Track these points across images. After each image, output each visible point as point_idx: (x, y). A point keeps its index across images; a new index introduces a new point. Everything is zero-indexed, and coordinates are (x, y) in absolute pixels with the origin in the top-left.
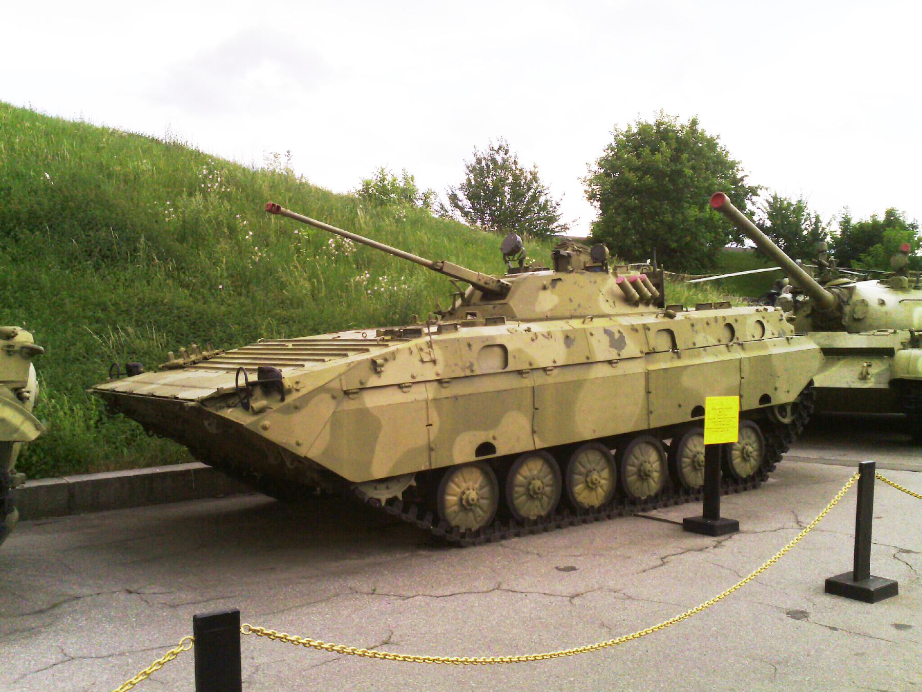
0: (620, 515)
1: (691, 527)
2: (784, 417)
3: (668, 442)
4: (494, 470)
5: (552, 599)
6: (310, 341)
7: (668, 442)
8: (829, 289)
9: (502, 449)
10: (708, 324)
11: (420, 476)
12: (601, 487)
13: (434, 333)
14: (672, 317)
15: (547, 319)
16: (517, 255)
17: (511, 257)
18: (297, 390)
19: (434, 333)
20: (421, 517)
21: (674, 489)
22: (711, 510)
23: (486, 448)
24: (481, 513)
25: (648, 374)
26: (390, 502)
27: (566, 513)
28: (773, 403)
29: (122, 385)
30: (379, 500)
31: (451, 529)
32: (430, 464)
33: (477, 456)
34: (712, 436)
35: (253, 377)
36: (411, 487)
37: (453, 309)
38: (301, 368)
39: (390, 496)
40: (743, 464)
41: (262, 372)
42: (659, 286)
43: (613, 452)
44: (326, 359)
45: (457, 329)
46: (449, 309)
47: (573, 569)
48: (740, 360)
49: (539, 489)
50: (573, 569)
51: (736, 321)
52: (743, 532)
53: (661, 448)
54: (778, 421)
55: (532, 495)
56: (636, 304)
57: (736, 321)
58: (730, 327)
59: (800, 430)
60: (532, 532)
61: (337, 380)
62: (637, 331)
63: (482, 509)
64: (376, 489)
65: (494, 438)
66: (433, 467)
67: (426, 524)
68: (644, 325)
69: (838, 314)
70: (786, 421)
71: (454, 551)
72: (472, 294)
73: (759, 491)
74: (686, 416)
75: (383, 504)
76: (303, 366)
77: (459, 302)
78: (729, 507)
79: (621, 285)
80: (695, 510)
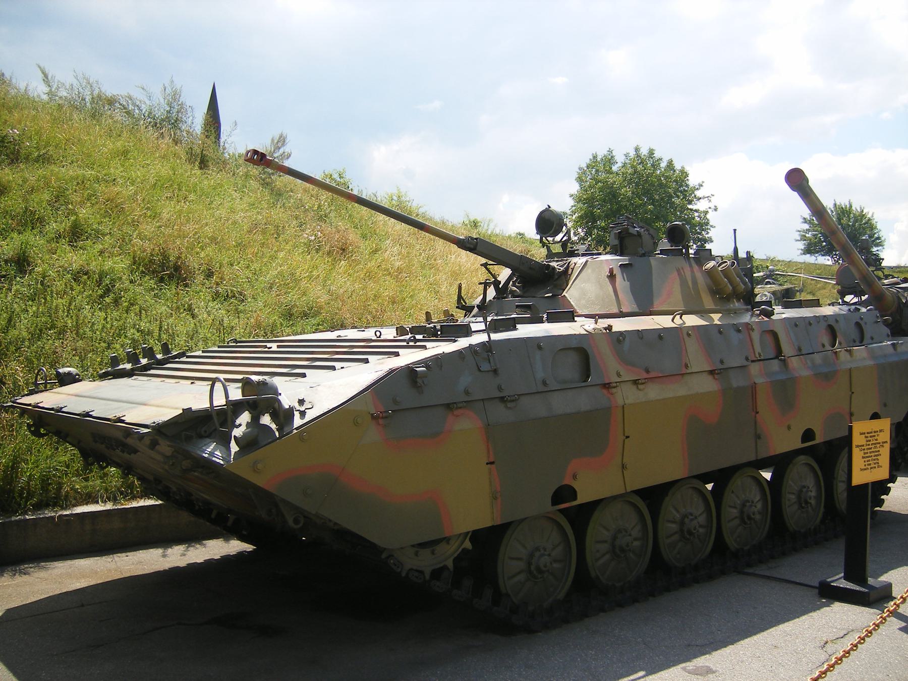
10: (356, 424)
11: (476, 536)
15: (158, 406)
23: (564, 493)
29: (49, 399)
30: (421, 572)
33: (802, 443)
35: (236, 393)
38: (300, 379)
41: (247, 384)
49: (545, 566)
55: (745, 518)
66: (759, 458)
69: (583, 401)
75: (427, 577)
76: (304, 375)
77: (491, 293)
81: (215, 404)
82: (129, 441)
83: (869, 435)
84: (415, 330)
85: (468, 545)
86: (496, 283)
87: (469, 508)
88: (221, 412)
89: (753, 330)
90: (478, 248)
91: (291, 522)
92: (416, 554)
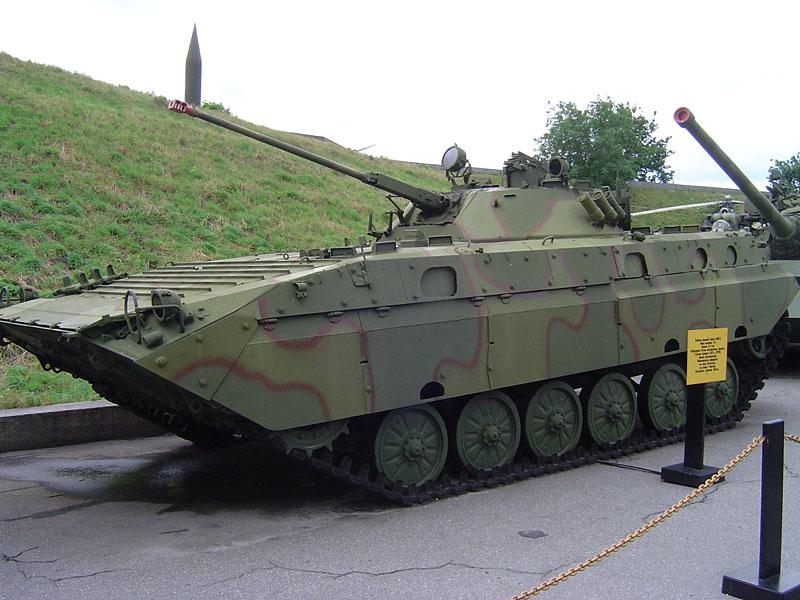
0: (587, 463)
2: (758, 351)
3: (637, 379)
4: (440, 412)
5: (520, 576)
6: (234, 263)
7: (637, 379)
9: (451, 392)
10: (680, 248)
11: (354, 422)
13: (368, 253)
14: (641, 239)
16: (462, 171)
17: (455, 174)
19: (368, 253)
20: (355, 471)
21: (646, 435)
22: (694, 456)
25: (586, 307)
26: (318, 453)
27: (527, 463)
28: (750, 335)
33: (422, 398)
36: (342, 434)
37: (390, 229)
39: (316, 447)
40: (717, 403)
43: (579, 390)
44: (238, 281)
46: (385, 229)
47: (542, 534)
48: (715, 288)
51: (709, 245)
53: (632, 388)
54: (754, 355)
56: (600, 224)
58: (703, 253)
60: (487, 486)
62: (605, 254)
64: (300, 438)
70: (761, 355)
71: (394, 512)
72: (411, 212)
73: (734, 432)
74: (658, 351)
75: (310, 454)
77: (396, 221)
79: (586, 203)
80: (675, 456)
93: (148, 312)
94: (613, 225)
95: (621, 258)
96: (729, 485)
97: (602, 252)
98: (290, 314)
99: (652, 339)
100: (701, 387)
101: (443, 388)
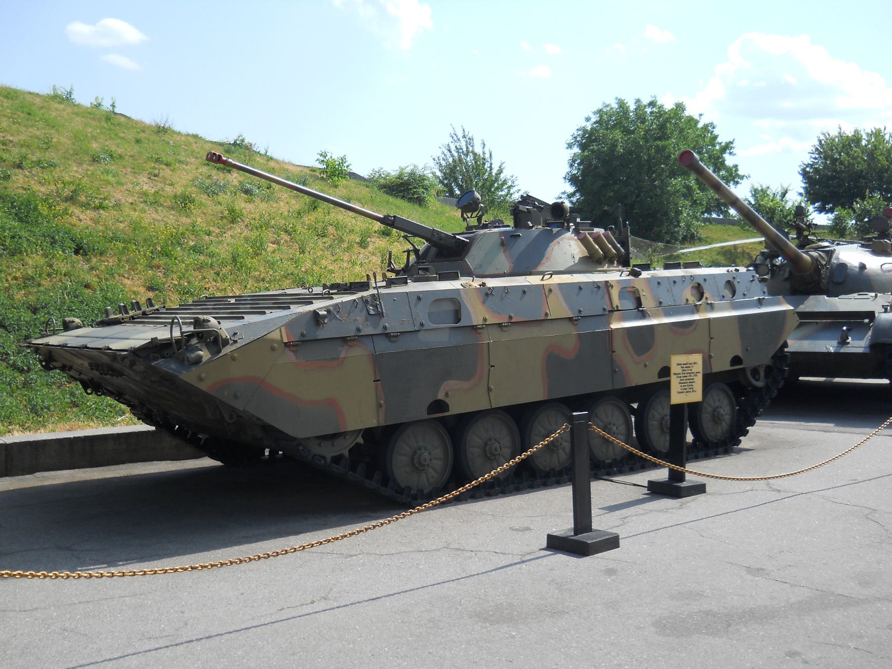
1: (657, 490)
2: (757, 380)
8: (806, 253)
9: (456, 408)
11: (368, 433)
12: (563, 449)
18: (235, 342)
23: (439, 406)
24: (434, 474)
30: (324, 458)
31: (400, 491)
32: (378, 421)
34: (677, 398)
36: (358, 444)
42: (624, 244)
45: (407, 283)
47: (528, 529)
50: (528, 529)
52: (711, 494)
54: (751, 385)
57: (705, 280)
59: (775, 393)
61: (278, 331)
63: (434, 469)
65: (447, 395)
66: (616, 388)
67: (372, 484)
68: (607, 282)
70: (760, 384)
75: (329, 460)
77: (413, 257)
78: (695, 471)
80: (661, 475)
81: (174, 335)
82: (117, 365)
83: (686, 366)
84: (333, 286)
85: (360, 440)
86: (416, 251)
87: (361, 413)
88: (178, 341)
89: (612, 286)
90: (396, 224)
91: (227, 418)
92: (320, 445)
93: (191, 336)
94: (611, 262)
95: (615, 293)
96: (708, 497)
97: (597, 286)
98: (311, 340)
99: (645, 366)
100: (681, 406)
101: (448, 405)
